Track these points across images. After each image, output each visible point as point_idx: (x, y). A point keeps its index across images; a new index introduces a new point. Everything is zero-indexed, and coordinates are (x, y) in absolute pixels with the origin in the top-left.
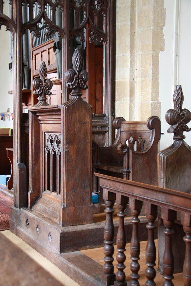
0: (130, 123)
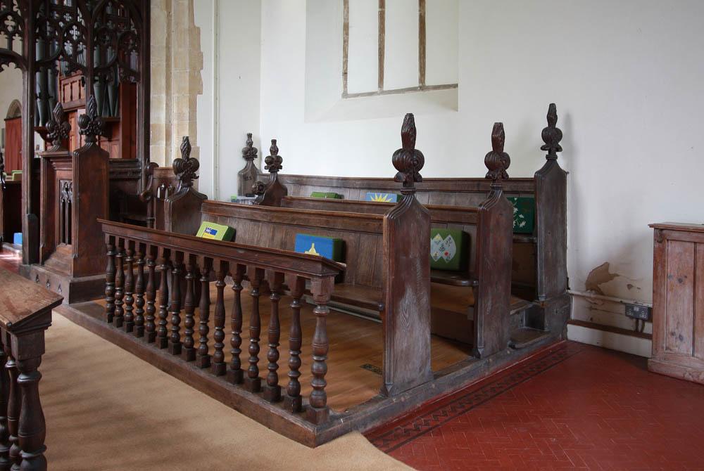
0: (163, 169)
